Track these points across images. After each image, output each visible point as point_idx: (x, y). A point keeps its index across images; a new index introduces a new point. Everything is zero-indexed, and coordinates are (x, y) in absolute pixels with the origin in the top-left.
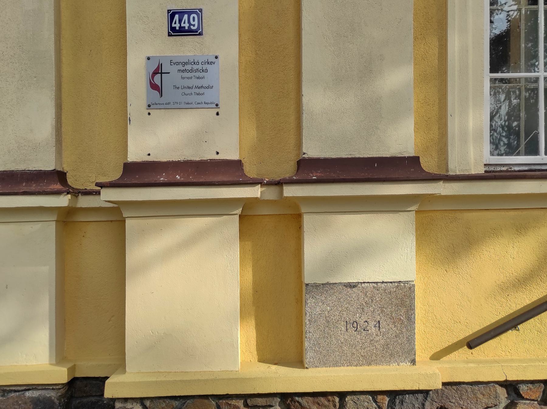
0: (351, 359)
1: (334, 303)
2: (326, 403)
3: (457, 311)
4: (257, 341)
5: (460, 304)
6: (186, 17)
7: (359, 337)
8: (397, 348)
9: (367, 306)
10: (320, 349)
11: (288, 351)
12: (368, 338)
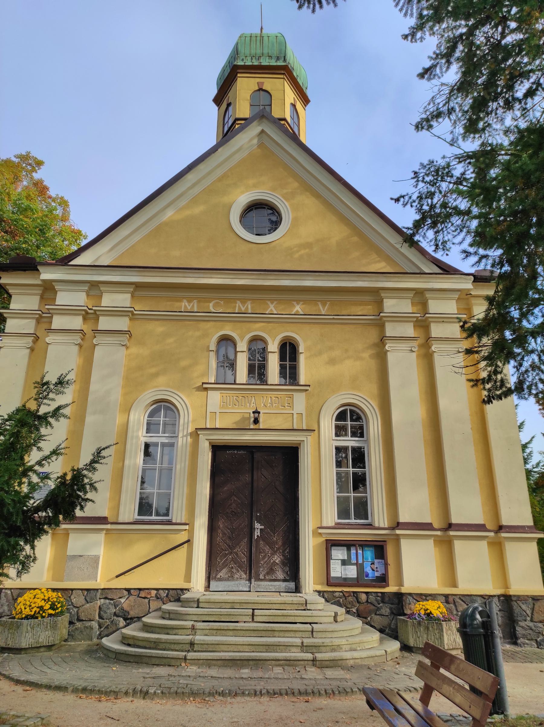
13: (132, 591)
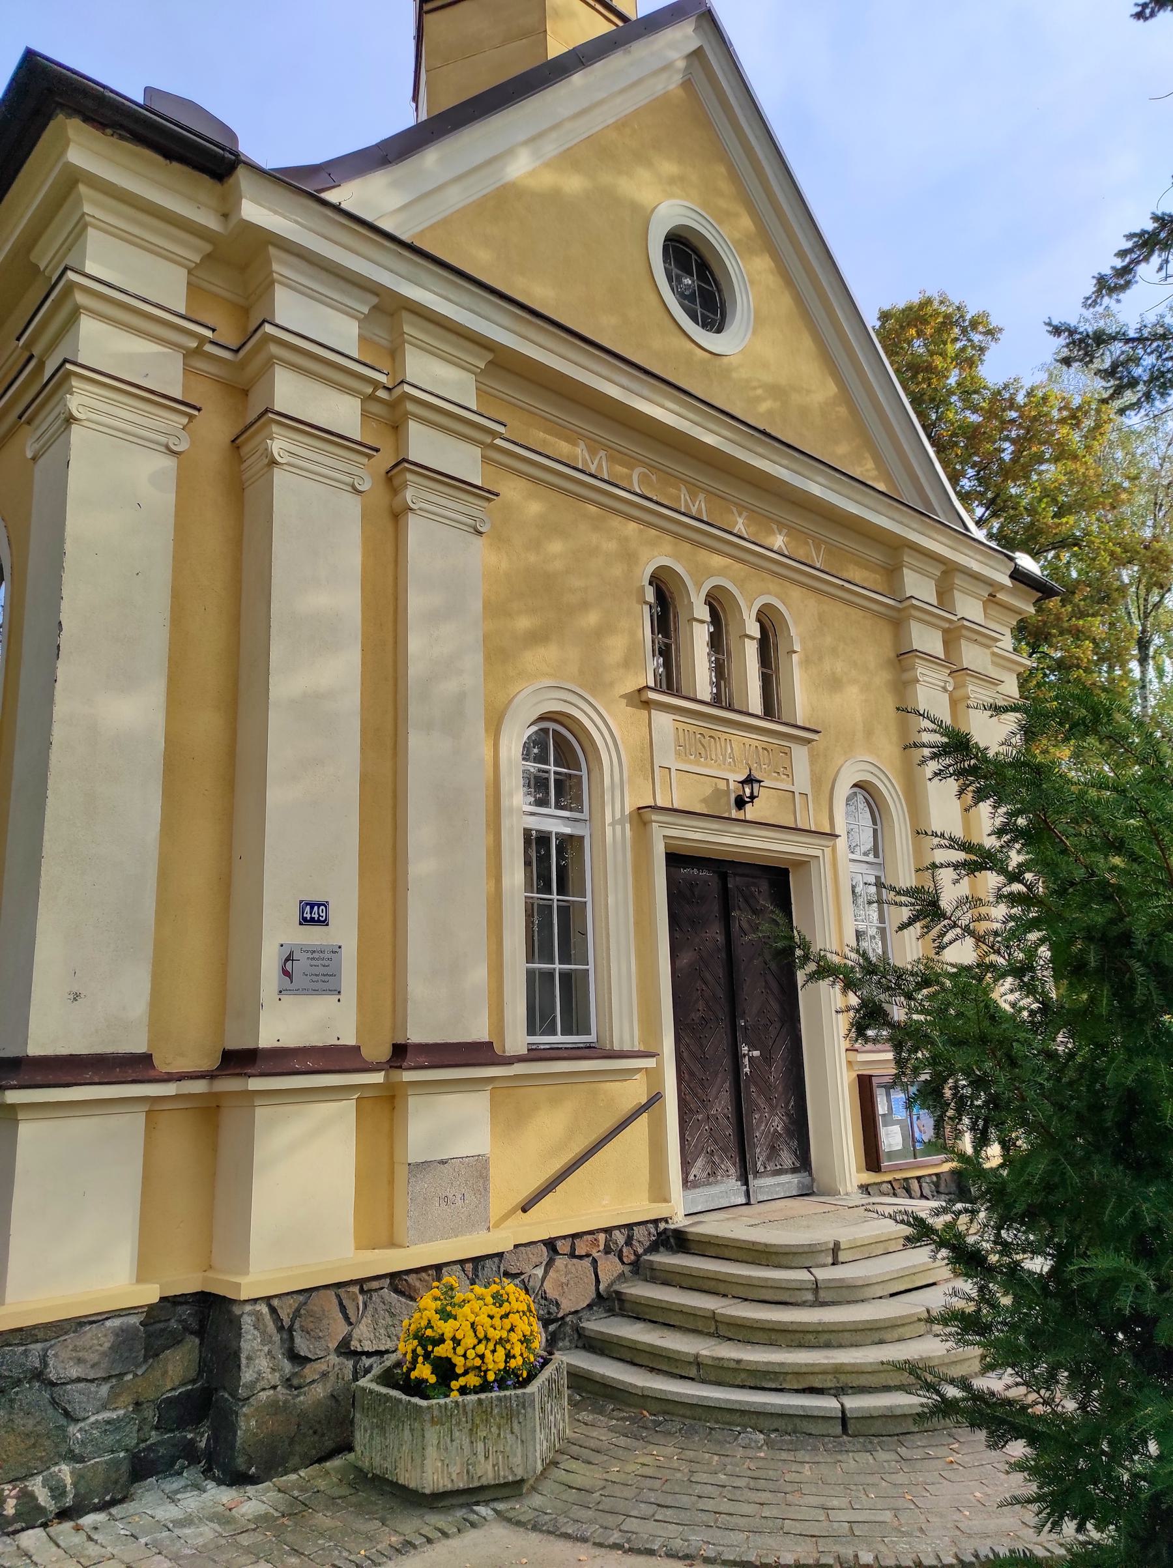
2: (427, 1278)
6: (316, 907)
13: (559, 1244)
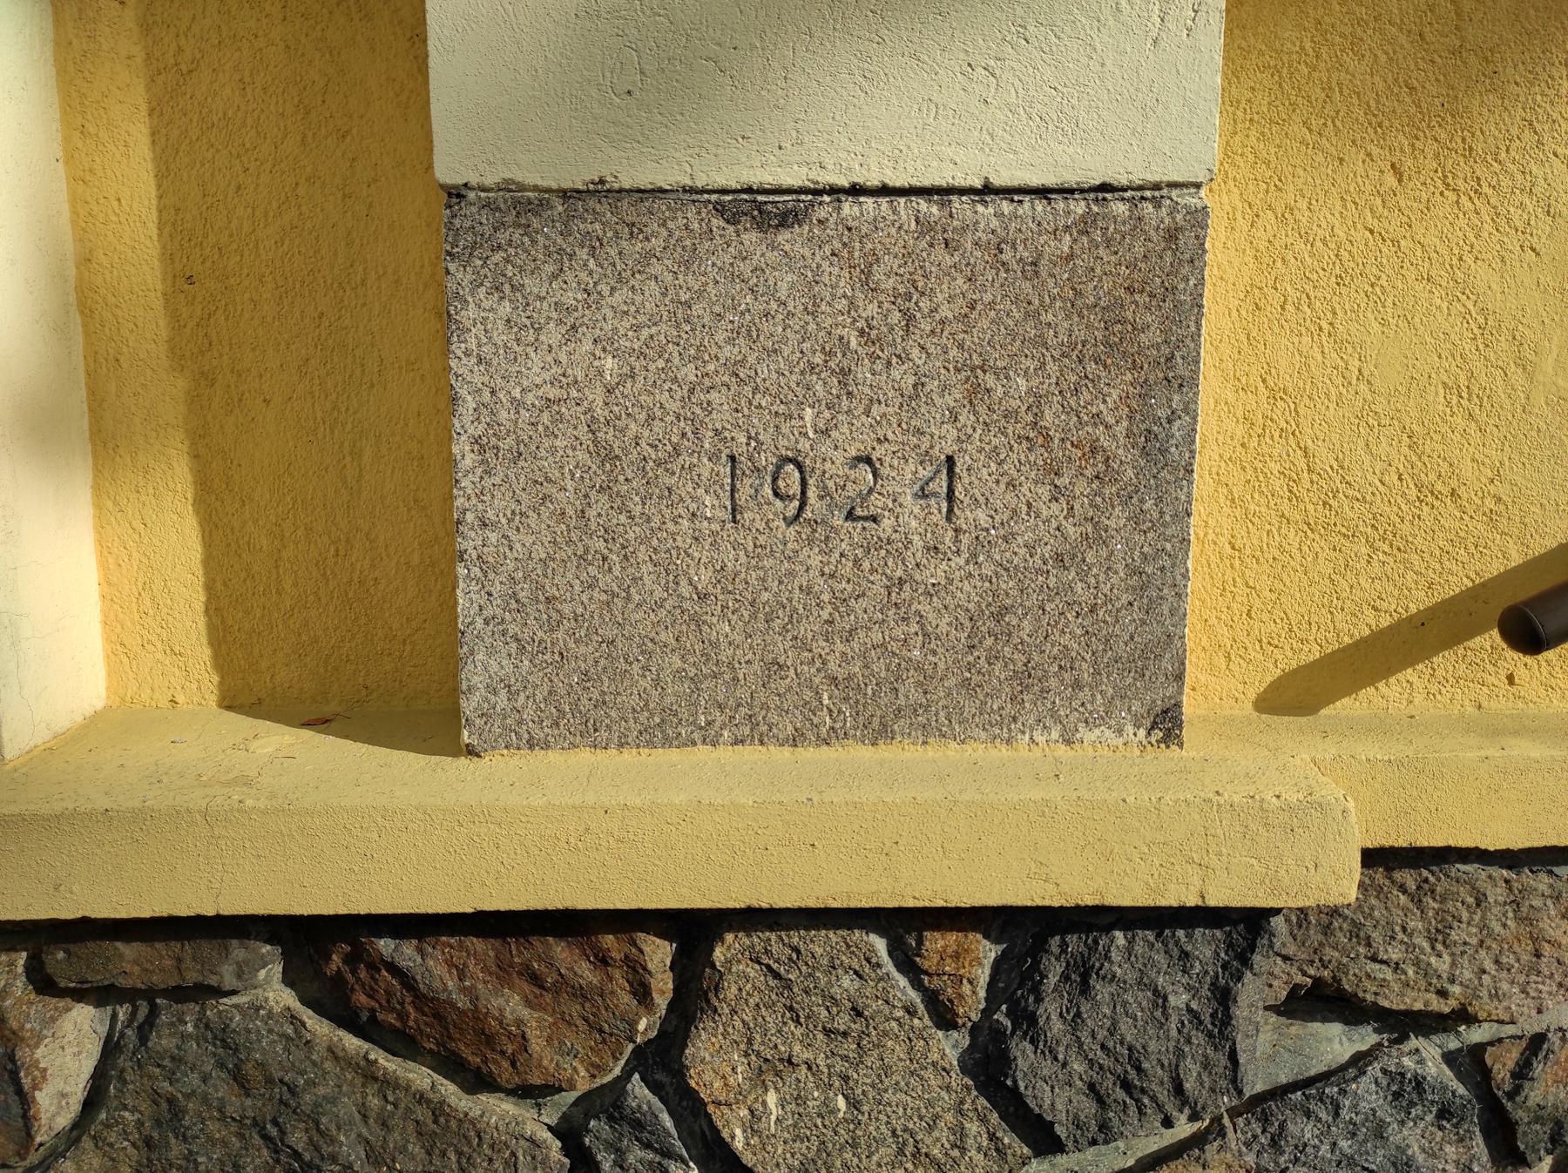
0: (762, 696)
1: (645, 333)
2: (586, 973)
3: (1445, 429)
4: (209, 587)
5: (1463, 382)
7: (815, 561)
8: (1063, 632)
9: (874, 358)
10: (560, 635)
11: (408, 648)
12: (873, 570)
